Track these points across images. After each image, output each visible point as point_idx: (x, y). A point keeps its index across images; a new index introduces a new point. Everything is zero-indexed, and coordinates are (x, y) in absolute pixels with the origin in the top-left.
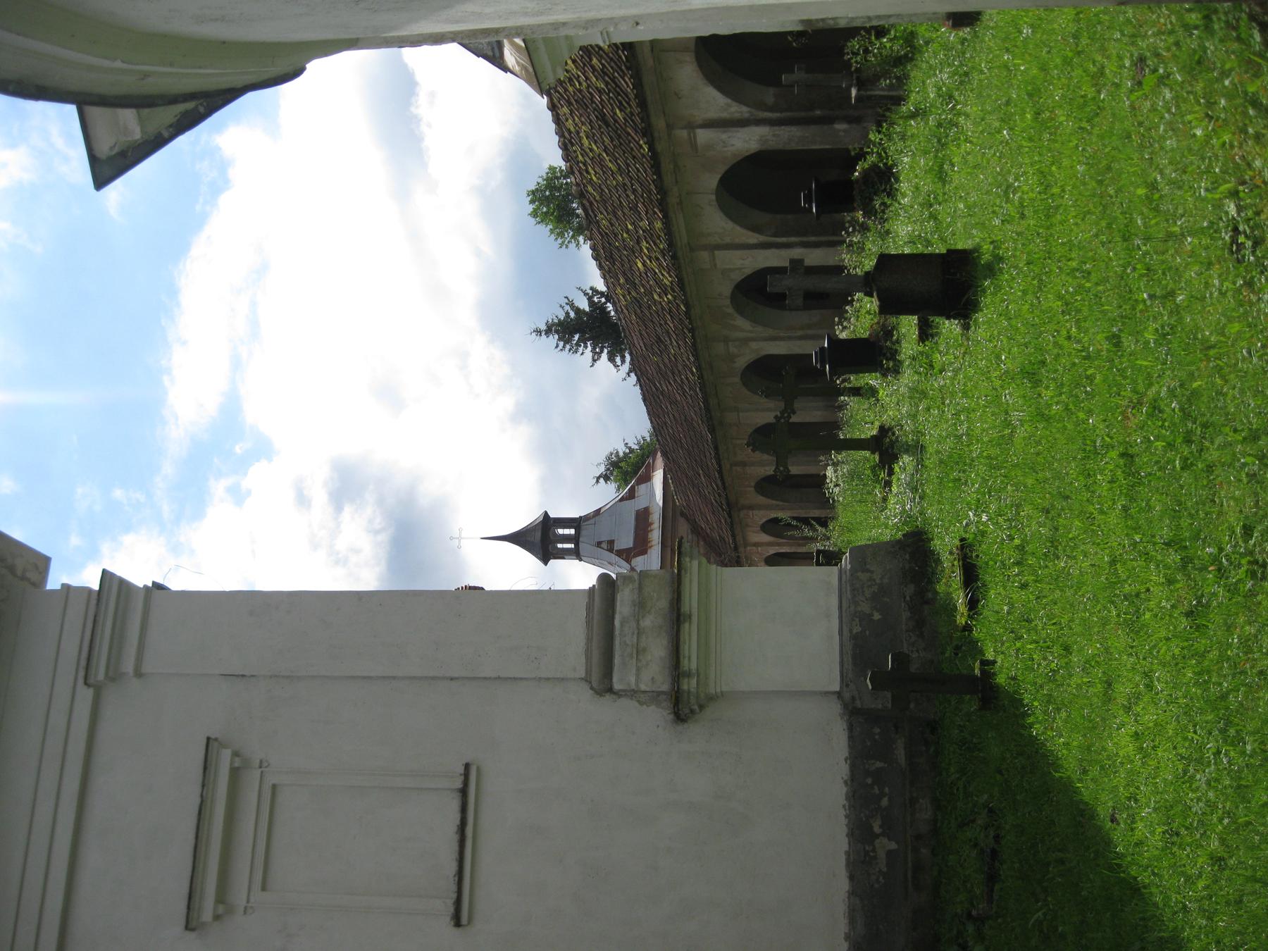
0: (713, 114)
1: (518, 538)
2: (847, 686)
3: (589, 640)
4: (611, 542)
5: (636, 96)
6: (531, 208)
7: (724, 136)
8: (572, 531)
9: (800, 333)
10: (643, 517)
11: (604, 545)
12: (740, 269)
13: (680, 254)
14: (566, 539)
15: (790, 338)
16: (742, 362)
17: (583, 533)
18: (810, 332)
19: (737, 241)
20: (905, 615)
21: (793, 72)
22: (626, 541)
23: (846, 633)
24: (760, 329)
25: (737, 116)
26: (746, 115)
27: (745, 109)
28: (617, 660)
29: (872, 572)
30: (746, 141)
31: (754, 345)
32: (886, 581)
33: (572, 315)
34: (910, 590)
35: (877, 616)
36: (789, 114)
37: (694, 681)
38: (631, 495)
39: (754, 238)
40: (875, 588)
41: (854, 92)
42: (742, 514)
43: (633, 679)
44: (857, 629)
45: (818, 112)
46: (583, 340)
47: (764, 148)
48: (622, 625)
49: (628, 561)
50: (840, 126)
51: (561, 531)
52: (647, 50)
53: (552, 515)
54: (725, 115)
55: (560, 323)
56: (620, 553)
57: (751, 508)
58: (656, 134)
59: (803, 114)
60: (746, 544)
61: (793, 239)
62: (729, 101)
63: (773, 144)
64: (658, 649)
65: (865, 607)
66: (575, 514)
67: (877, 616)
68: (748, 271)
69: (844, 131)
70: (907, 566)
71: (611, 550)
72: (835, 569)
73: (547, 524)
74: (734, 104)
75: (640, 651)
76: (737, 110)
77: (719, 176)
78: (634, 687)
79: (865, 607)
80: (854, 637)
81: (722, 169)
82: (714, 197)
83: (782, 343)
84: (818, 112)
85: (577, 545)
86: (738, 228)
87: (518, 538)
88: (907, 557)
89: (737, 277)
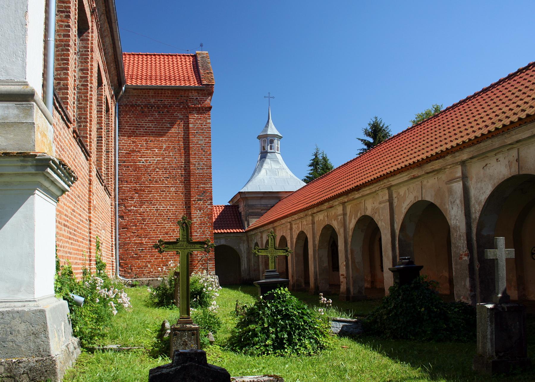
0: (473, 192)
7: (458, 201)
9: (349, 256)
18: (350, 262)
19: (396, 216)
21: (507, 307)
24: (351, 233)
25: (473, 210)
26: (473, 216)
27: (478, 215)
30: (455, 216)
39: (397, 227)
41: (490, 306)
47: (452, 230)
52: (30, 121)
54: (473, 201)
58: (457, 154)
61: (398, 251)
62: (483, 204)
63: (454, 235)
69: (465, 285)
74: (481, 206)
76: (476, 210)
77: (433, 202)
81: (437, 204)
83: (343, 247)
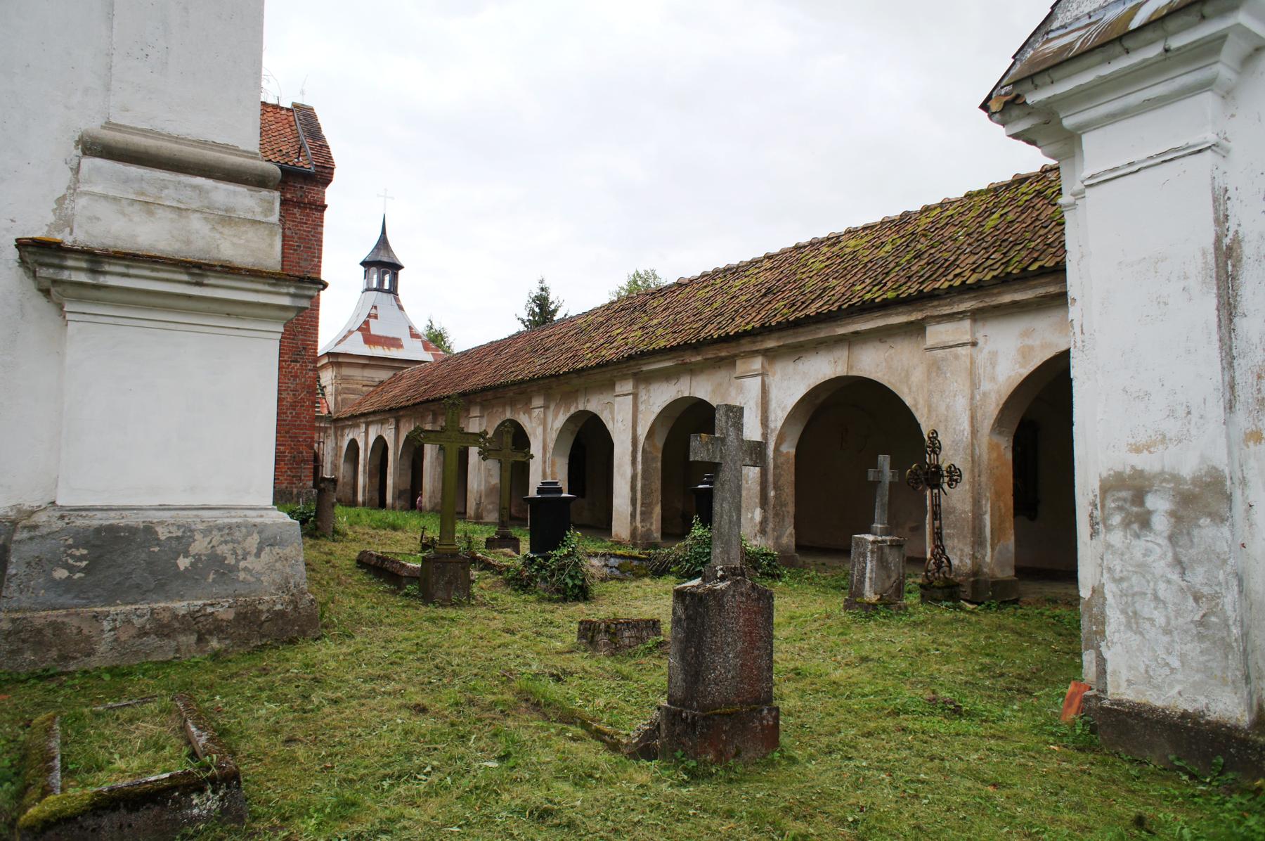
0: (774, 394)
1: (383, 242)
2: (62, 517)
3: (176, 139)
4: (376, 317)
5: (807, 316)
6: (642, 272)
8: (386, 286)
10: (394, 343)
11: (374, 311)
12: (613, 419)
13: (632, 363)
14: (381, 282)
15: (544, 462)
16: (523, 419)
17: (385, 295)
19: (640, 416)
20: (181, 606)
22: (376, 329)
23: (155, 516)
24: (555, 436)
25: (772, 417)
27: (779, 424)
28: (134, 170)
29: (258, 555)
31: (540, 430)
32: (242, 575)
33: (552, 307)
34: (225, 613)
35: (183, 563)
36: (771, 466)
37: (83, 278)
38: (414, 335)
39: (643, 432)
40: (231, 560)
41: (870, 538)
42: (392, 420)
43: (98, 189)
44: (163, 534)
45: (772, 493)
46: (534, 314)
48: (195, 187)
49: (359, 329)
50: (758, 515)
51: (387, 278)
53: (400, 272)
55: (546, 299)
56: (366, 323)
57: (397, 428)
59: (771, 478)
60: (368, 425)
61: (639, 467)
62: (789, 409)
64: (150, 234)
65: (200, 546)
66: (400, 291)
67: (183, 563)
68: (609, 427)
69: (752, 518)
70: (263, 607)
71: (369, 316)
72: (268, 501)
73: (394, 268)
75: (148, 206)
78: (83, 188)
79: (200, 546)
80: (149, 530)
82: (686, 394)
84: (772, 493)
85: (375, 290)
86: (653, 417)
87: (383, 242)
88: (278, 607)
89: (605, 417)
